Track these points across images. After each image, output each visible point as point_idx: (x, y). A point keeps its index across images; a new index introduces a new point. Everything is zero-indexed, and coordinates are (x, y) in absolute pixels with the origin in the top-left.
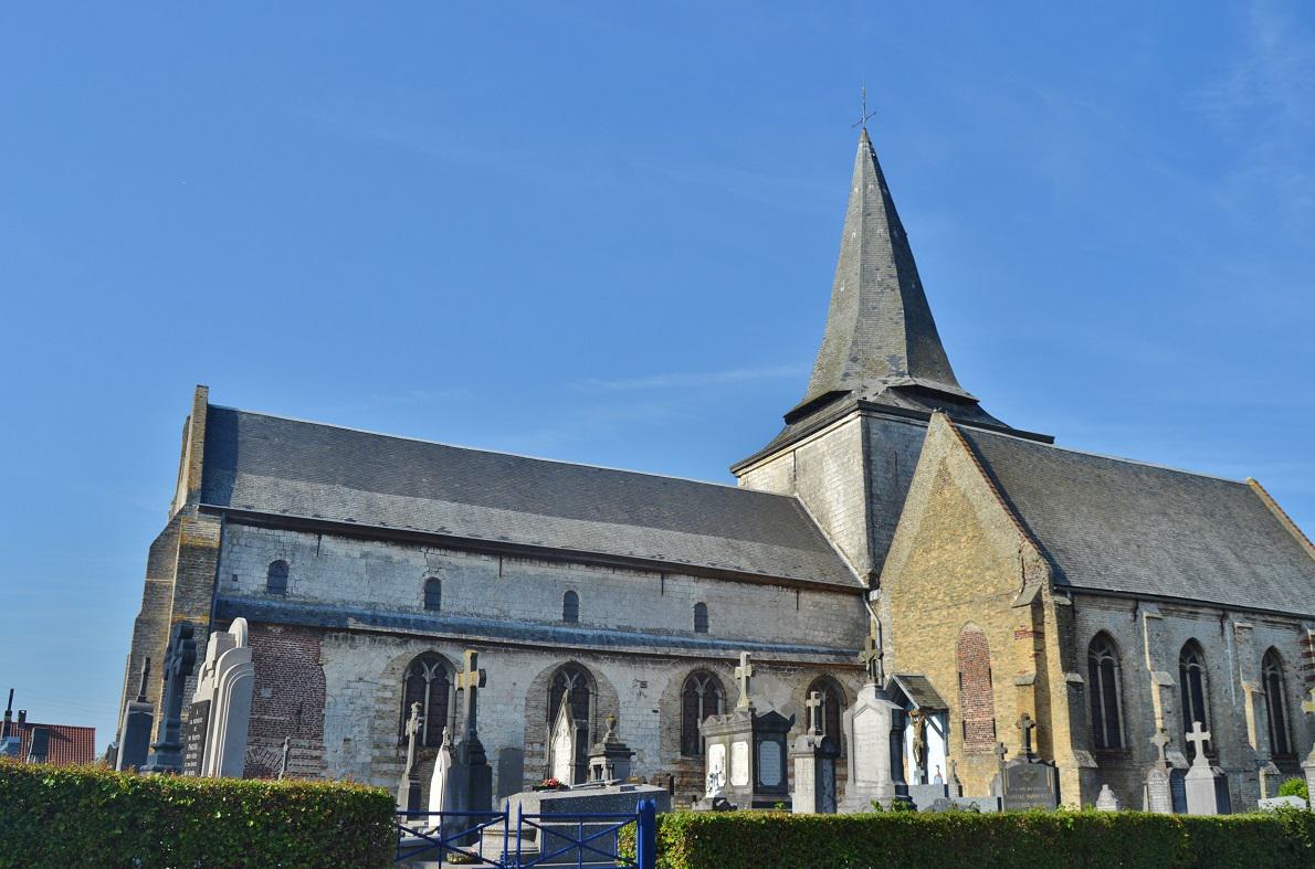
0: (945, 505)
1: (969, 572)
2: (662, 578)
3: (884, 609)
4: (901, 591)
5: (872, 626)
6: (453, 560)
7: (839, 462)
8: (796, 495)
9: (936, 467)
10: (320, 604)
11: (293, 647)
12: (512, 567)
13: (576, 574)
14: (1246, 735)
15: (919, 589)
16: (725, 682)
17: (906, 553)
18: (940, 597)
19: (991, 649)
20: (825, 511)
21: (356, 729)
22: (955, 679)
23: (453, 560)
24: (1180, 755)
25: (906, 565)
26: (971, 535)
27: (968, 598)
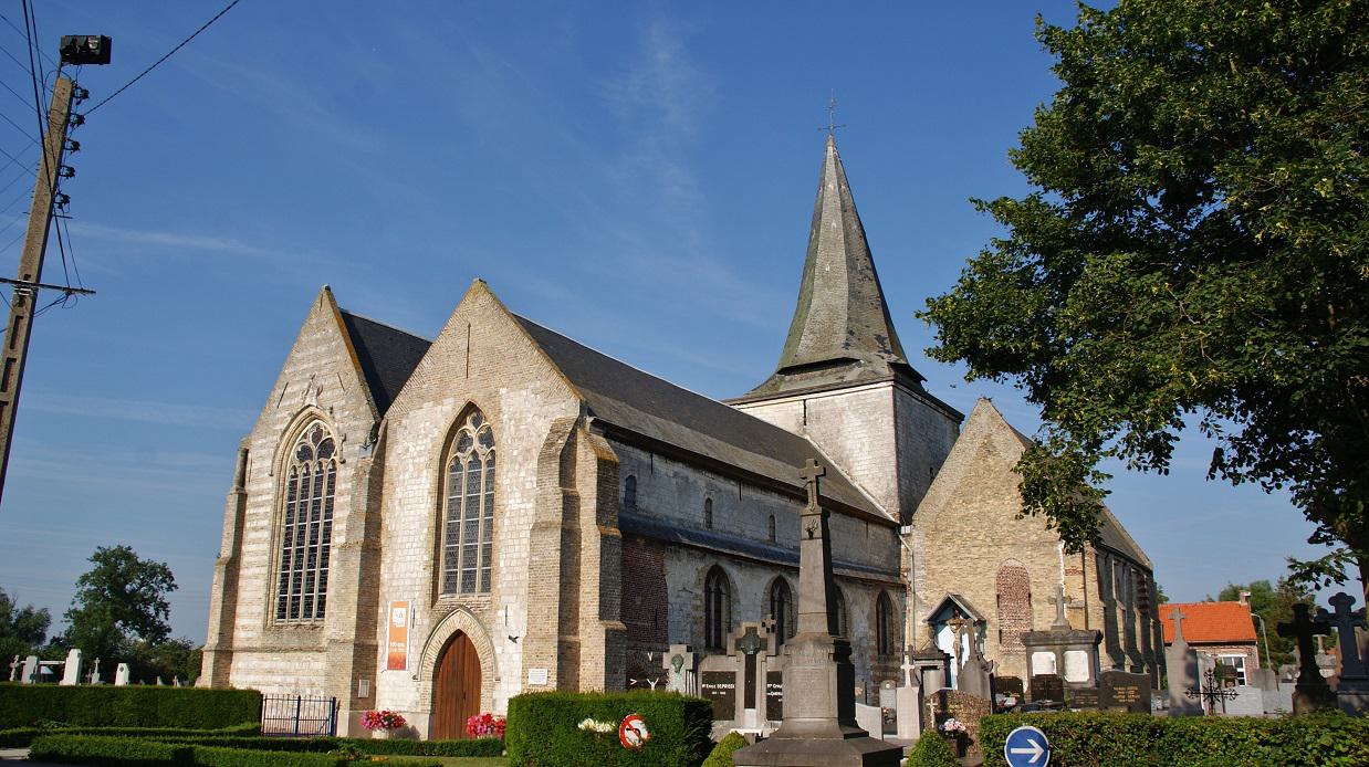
0: (989, 469)
3: (916, 541)
5: (903, 553)
6: (718, 483)
7: (864, 418)
8: (807, 437)
9: (979, 441)
10: (654, 519)
12: (751, 494)
13: (773, 500)
14: (1135, 643)
15: (958, 530)
17: (944, 501)
19: (1032, 580)
20: (844, 456)
21: (685, 633)
22: (994, 599)
23: (718, 483)
24: (1325, 676)
27: (1010, 542)
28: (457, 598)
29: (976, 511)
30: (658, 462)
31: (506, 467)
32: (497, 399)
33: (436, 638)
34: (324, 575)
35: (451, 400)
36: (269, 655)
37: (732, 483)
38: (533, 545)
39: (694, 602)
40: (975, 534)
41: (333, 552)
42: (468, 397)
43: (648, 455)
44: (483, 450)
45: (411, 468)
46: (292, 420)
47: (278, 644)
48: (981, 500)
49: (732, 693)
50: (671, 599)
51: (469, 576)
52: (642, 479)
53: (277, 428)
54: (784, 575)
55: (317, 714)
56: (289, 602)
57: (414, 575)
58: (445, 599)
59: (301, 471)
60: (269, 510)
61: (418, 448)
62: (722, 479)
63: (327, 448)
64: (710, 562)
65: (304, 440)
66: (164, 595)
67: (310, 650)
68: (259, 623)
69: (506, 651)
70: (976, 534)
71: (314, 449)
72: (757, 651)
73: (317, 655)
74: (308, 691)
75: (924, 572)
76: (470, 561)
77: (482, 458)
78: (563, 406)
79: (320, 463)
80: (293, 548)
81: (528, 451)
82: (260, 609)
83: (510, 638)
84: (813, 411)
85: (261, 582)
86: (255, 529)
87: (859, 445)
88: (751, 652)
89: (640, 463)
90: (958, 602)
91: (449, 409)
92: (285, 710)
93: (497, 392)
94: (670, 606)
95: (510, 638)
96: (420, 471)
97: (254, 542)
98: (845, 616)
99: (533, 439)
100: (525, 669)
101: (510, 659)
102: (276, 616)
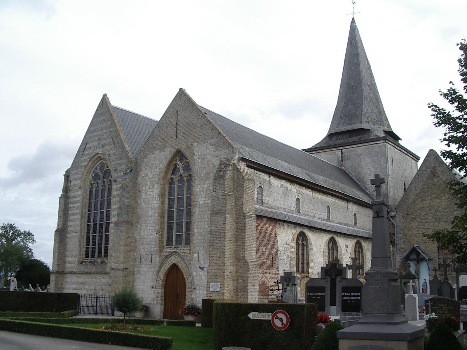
1: (445, 210)
2: (347, 203)
4: (408, 214)
6: (302, 190)
11: (269, 227)
12: (319, 196)
13: (329, 199)
15: (418, 214)
16: (363, 246)
17: (412, 200)
18: (430, 218)
20: (362, 177)
21: (286, 265)
25: (412, 204)
26: (447, 197)
27: (444, 220)
28: (173, 249)
29: (428, 205)
30: (273, 180)
31: (197, 182)
32: (192, 149)
33: (163, 268)
34: (107, 237)
35: (169, 149)
36: (81, 276)
37: (309, 190)
38: (211, 222)
39: (291, 250)
40: (427, 216)
41: (111, 225)
42: (177, 147)
43: (268, 176)
44: (185, 175)
45: (149, 183)
46: (90, 161)
47: (85, 270)
48: (430, 199)
49: (323, 298)
50: (280, 249)
51: (179, 237)
52: (266, 187)
53: (83, 164)
54: (335, 236)
55: (105, 304)
56: (90, 250)
57: (151, 236)
58: (167, 251)
59: (95, 186)
60: (79, 205)
61: (152, 174)
62: (304, 188)
63: (107, 173)
64: (299, 230)
65: (96, 171)
66: (30, 245)
67: (101, 273)
68: (76, 260)
69: (198, 274)
70: (428, 216)
71: (101, 175)
72: (336, 276)
73: (104, 276)
74: (101, 293)
75: (401, 235)
76: (179, 230)
77: (185, 179)
78: (226, 151)
79: (104, 182)
80: (92, 224)
81: (208, 174)
82: (77, 253)
83: (200, 268)
84: (346, 155)
85: (77, 240)
86: (73, 214)
87: (369, 172)
88: (333, 277)
89: (264, 180)
90: (418, 250)
91: (167, 153)
92: (90, 302)
93: (192, 145)
94: (279, 252)
95: (200, 268)
96: (154, 186)
97: (72, 220)
98: (363, 257)
99: (211, 168)
100: (208, 283)
101: (200, 278)
102: (84, 256)
